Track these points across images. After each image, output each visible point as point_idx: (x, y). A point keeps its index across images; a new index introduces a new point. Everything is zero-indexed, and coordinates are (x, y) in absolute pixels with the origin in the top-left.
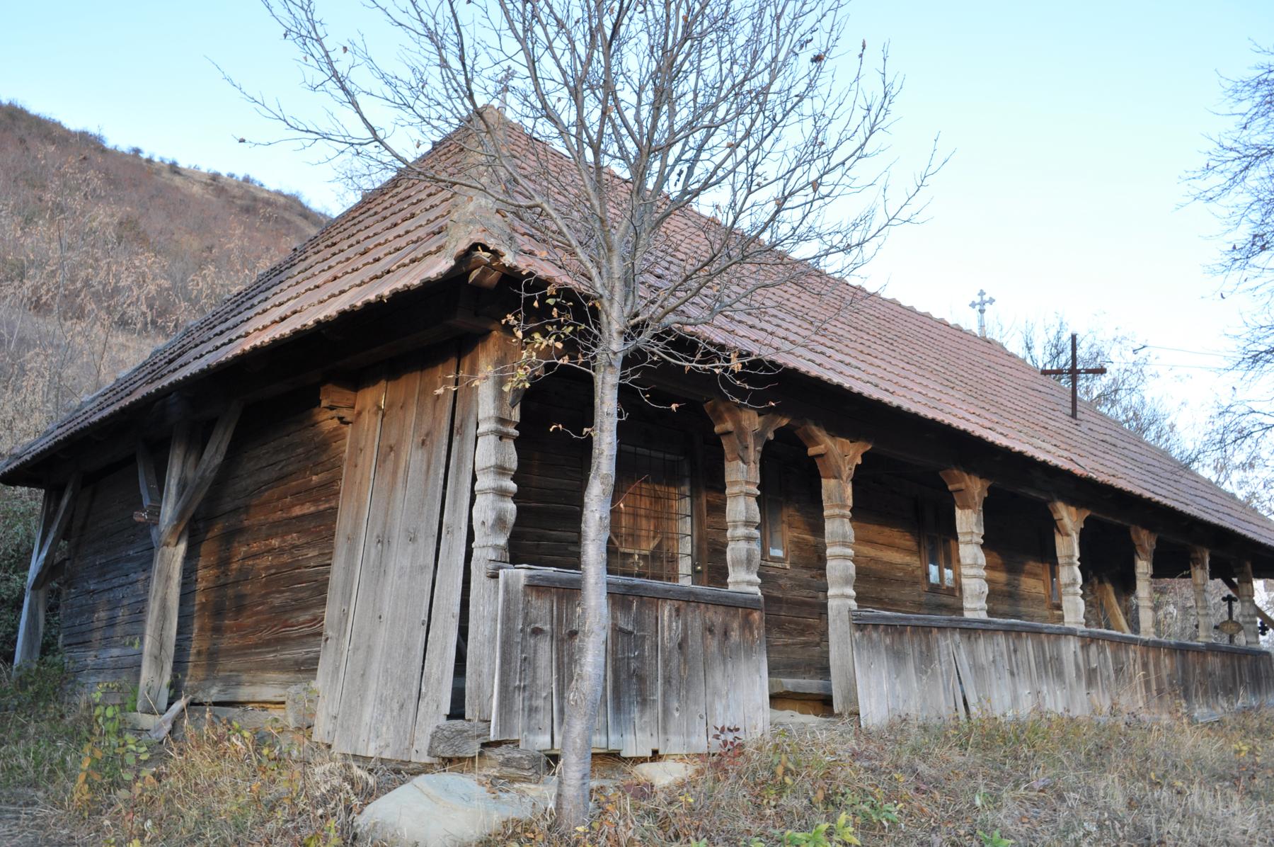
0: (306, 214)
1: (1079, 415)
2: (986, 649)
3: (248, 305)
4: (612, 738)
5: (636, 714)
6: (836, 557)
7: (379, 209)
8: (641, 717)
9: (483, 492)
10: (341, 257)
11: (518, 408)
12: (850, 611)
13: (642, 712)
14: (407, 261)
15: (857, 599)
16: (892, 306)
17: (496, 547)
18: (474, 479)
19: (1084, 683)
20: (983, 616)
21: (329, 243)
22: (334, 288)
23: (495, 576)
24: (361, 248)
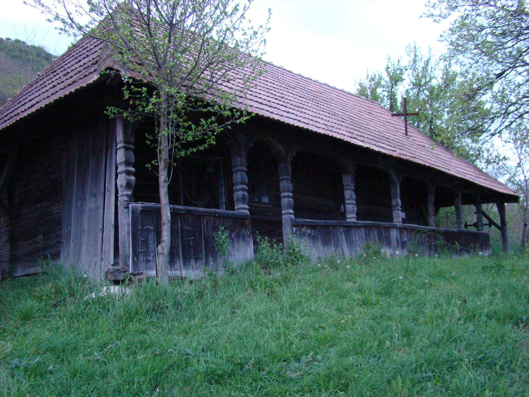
0: (48, 57)
1: (408, 133)
2: (358, 235)
3: (18, 101)
4: (183, 272)
5: (193, 262)
6: (285, 197)
7: (74, 54)
8: (196, 264)
9: (121, 173)
10: (57, 77)
11: (133, 136)
12: (291, 220)
13: (196, 262)
14: (82, 77)
15: (294, 214)
16: (324, 86)
17: (127, 195)
18: (117, 168)
19: (400, 246)
20: (354, 220)
21: (53, 71)
22: (53, 91)
23: (127, 208)
24: (65, 72)
